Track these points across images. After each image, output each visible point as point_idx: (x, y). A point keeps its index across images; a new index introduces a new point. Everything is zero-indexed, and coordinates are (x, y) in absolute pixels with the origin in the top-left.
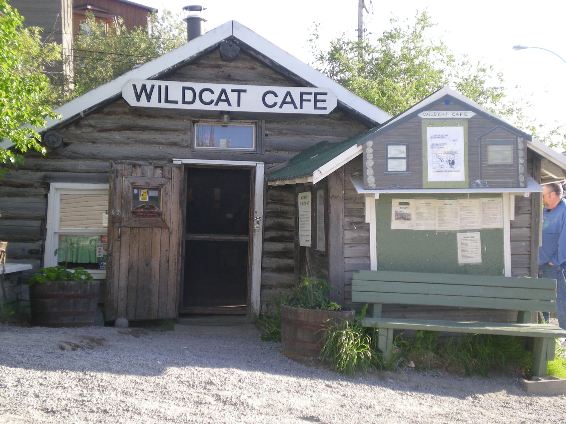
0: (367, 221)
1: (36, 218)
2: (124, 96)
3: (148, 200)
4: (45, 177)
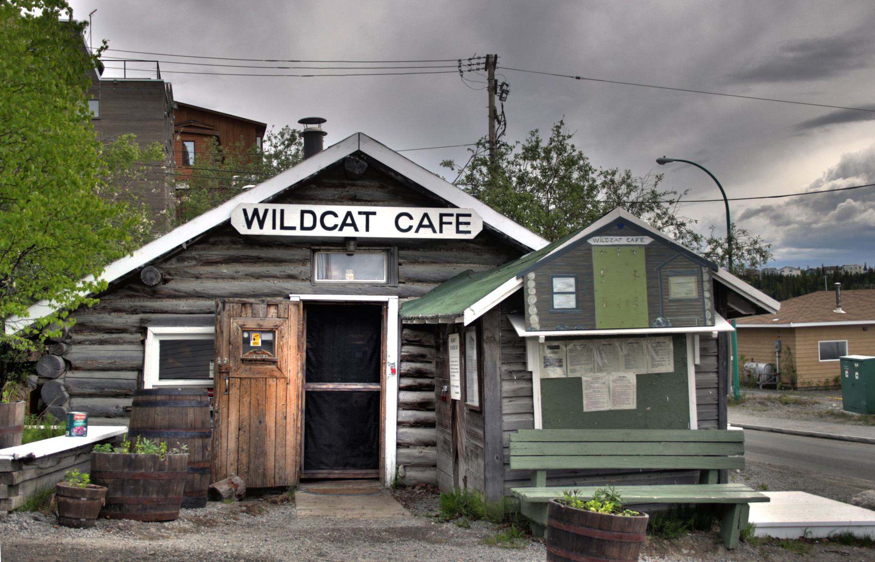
0: (530, 369)
1: (132, 369)
2: (233, 223)
3: (260, 345)
4: (142, 321)
